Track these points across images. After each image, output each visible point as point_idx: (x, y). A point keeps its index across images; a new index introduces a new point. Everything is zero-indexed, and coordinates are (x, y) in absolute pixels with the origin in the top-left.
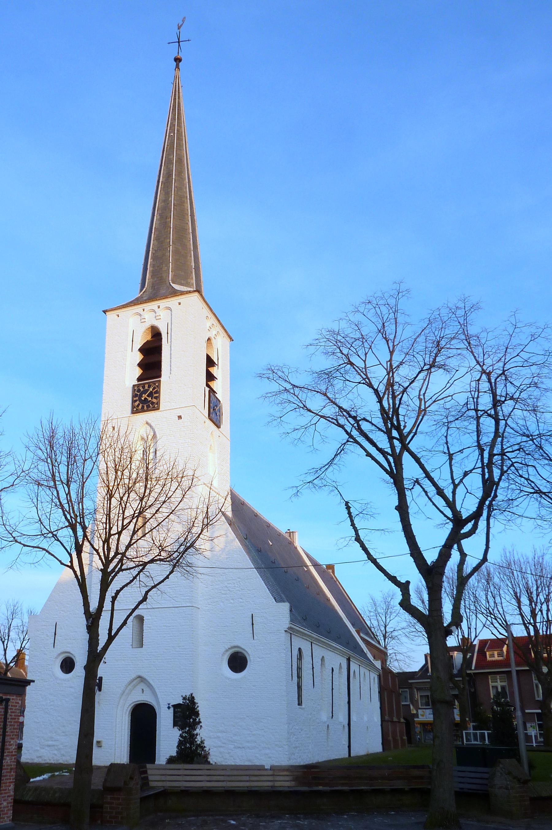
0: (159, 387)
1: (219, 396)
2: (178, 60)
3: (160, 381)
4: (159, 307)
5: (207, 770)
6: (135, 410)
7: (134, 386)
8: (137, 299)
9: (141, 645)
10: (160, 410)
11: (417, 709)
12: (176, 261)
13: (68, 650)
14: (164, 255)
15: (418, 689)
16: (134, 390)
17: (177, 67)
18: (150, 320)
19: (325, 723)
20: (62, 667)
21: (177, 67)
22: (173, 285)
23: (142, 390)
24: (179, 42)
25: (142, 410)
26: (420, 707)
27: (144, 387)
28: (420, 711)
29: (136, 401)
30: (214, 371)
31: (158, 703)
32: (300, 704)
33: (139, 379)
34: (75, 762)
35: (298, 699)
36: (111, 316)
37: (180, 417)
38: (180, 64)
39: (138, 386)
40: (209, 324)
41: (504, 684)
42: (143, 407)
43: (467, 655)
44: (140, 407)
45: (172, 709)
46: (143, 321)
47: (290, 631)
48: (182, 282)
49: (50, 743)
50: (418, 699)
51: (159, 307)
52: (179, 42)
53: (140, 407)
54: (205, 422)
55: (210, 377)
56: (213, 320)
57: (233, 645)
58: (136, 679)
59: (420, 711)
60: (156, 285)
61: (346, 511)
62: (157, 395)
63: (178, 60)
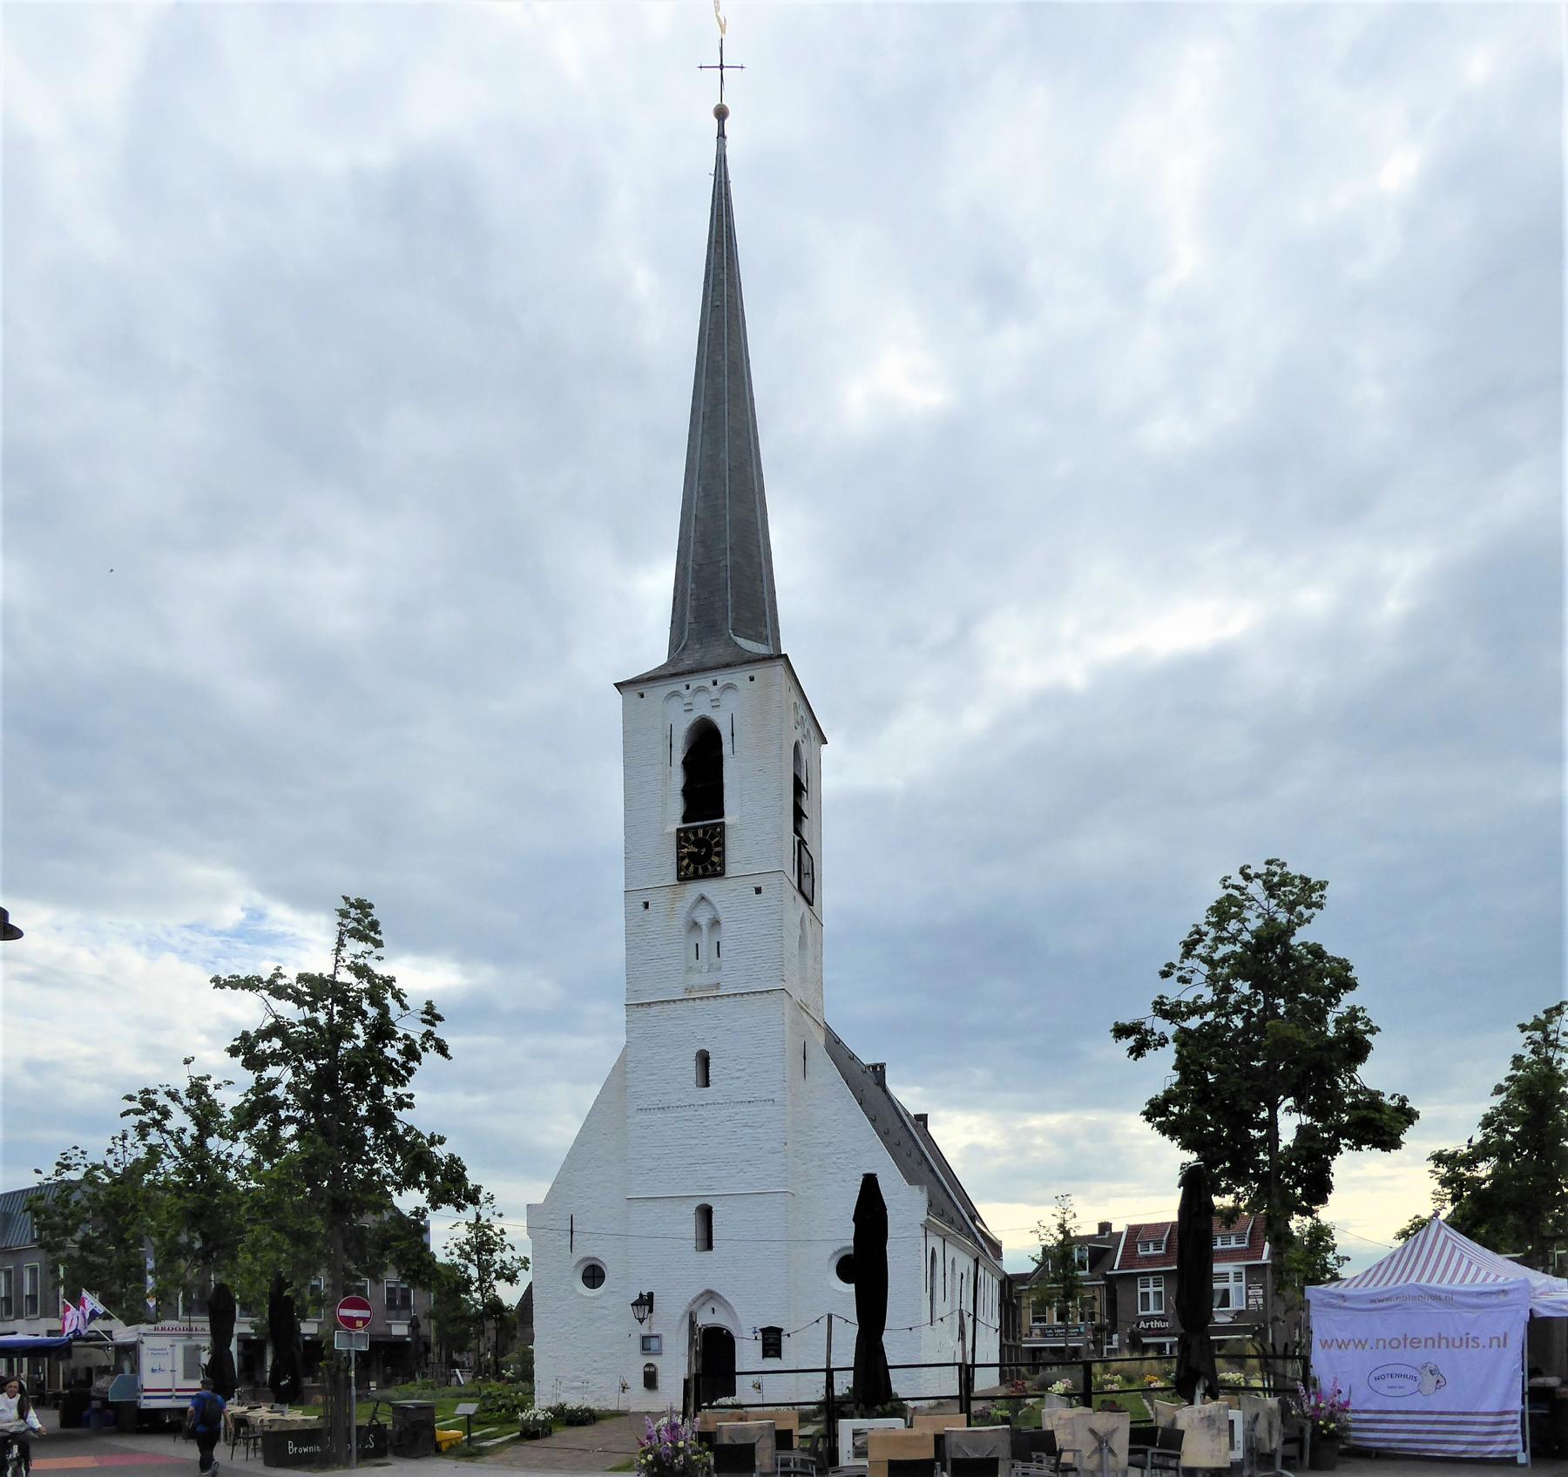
4: (715, 683)
6: (684, 877)
9: (709, 1246)
10: (731, 869)
13: (591, 1254)
16: (679, 839)
18: (702, 709)
20: (584, 1278)
22: (741, 642)
24: (722, 67)
25: (696, 877)
27: (696, 834)
33: (685, 819)
34: (1174, 1218)
37: (646, 905)
42: (696, 870)
43: (1272, 1255)
44: (691, 868)
45: (760, 1336)
46: (1495, 1342)
47: (927, 1227)
51: (715, 683)
52: (722, 67)
53: (691, 868)
61: (789, 838)
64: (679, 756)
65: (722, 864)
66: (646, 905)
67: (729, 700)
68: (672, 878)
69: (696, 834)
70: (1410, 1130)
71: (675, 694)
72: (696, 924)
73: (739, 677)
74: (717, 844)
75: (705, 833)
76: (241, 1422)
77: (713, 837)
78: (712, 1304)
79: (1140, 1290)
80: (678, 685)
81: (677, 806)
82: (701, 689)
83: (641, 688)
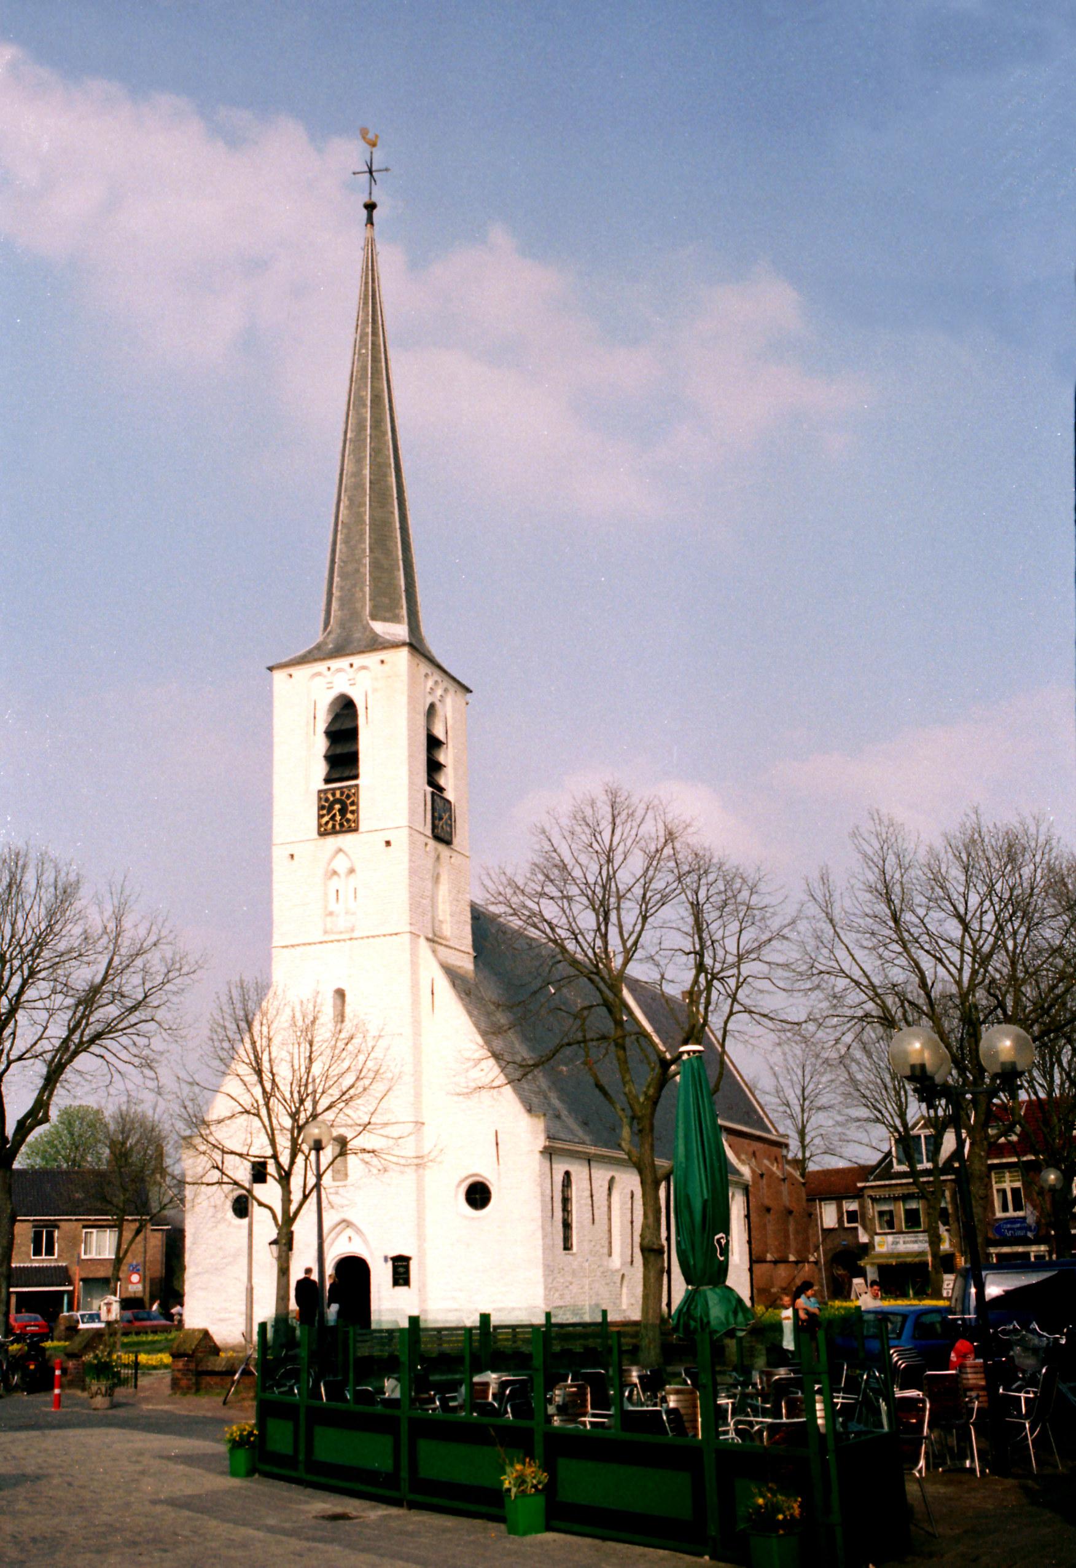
0: (356, 794)
1: (449, 795)
2: (370, 207)
3: (357, 786)
4: (351, 665)
5: (250, 1291)
7: (320, 792)
8: (318, 647)
10: (362, 828)
11: (873, 1234)
12: (374, 579)
14: (357, 571)
15: (874, 1200)
17: (370, 221)
19: (617, 1271)
21: (370, 221)
23: (331, 799)
25: (334, 832)
26: (878, 1231)
27: (334, 795)
28: (877, 1239)
29: (323, 816)
30: (442, 758)
31: (371, 1253)
32: (567, 1246)
33: (327, 781)
35: (252, 1302)
36: (279, 676)
37: (388, 843)
38: (375, 211)
39: (325, 791)
40: (430, 683)
41: (1018, 1184)
44: (330, 825)
45: (390, 1263)
48: (387, 615)
49: (222, 1316)
50: (874, 1217)
51: (351, 665)
54: (426, 844)
55: (434, 767)
56: (437, 676)
57: (471, 1172)
58: (339, 1224)
59: (877, 1239)
60: (345, 642)
62: (354, 808)
63: (370, 207)
64: (322, 724)
65: (356, 821)
66: (388, 843)
67: (363, 677)
68: (315, 835)
69: (334, 795)
70: (541, 1142)
71: (319, 674)
72: (335, 873)
73: (371, 659)
74: (353, 803)
75: (342, 794)
76: (82, 1316)
77: (327, 800)
78: (349, 1232)
79: (995, 1187)
80: (320, 667)
81: (321, 769)
82: (339, 670)
83: (291, 670)
